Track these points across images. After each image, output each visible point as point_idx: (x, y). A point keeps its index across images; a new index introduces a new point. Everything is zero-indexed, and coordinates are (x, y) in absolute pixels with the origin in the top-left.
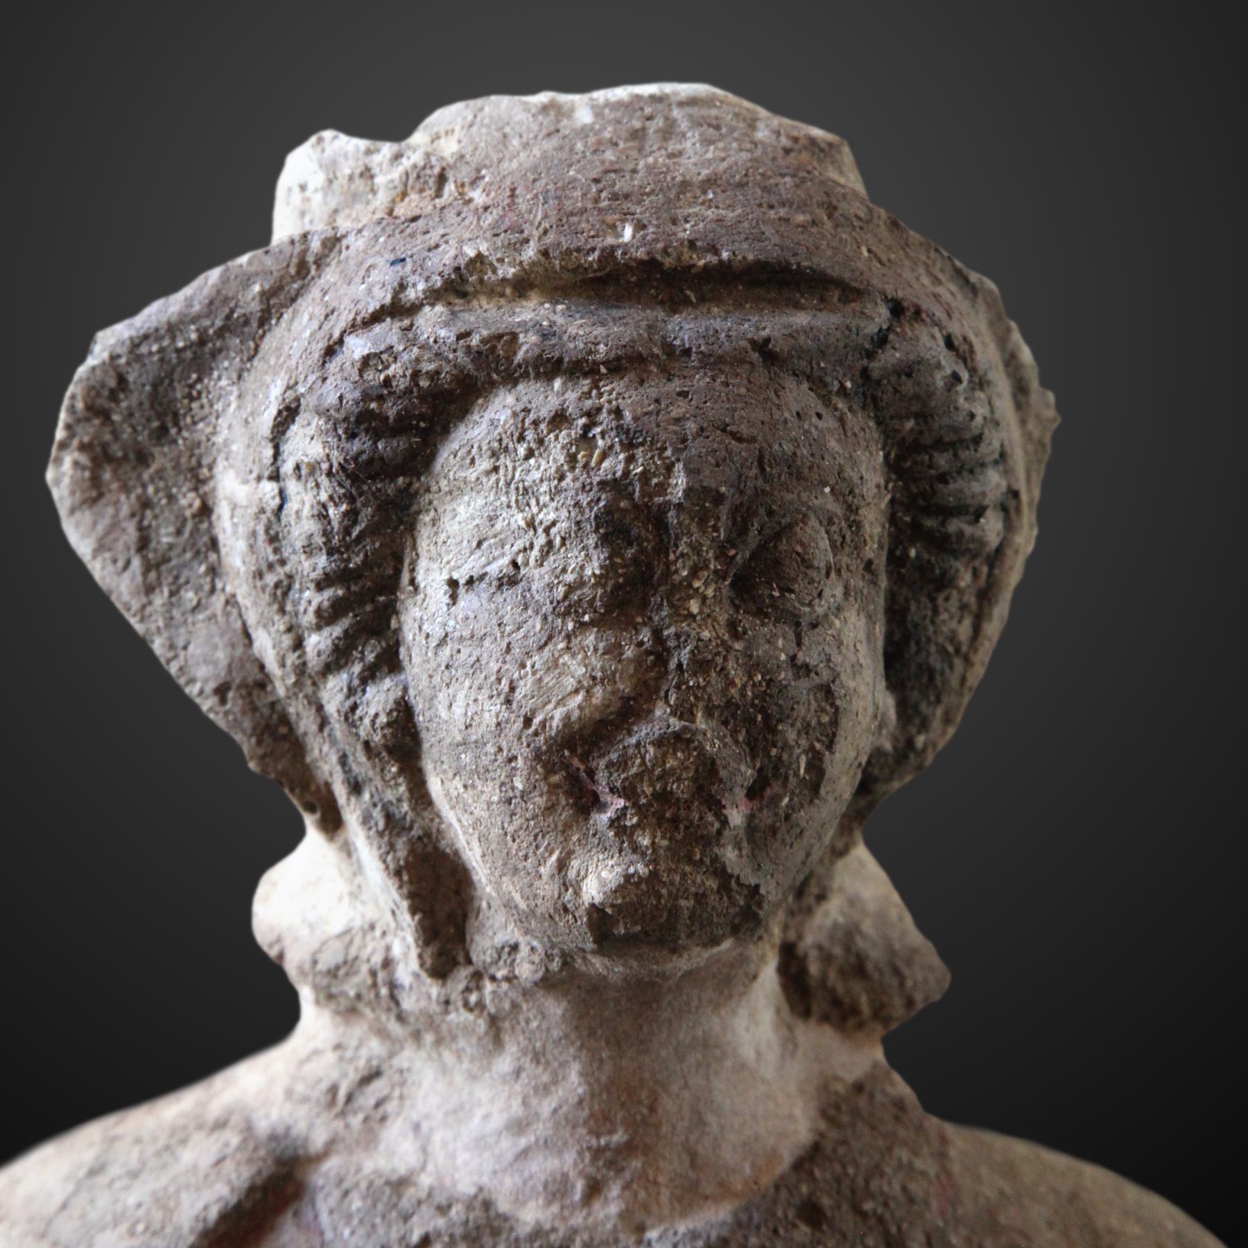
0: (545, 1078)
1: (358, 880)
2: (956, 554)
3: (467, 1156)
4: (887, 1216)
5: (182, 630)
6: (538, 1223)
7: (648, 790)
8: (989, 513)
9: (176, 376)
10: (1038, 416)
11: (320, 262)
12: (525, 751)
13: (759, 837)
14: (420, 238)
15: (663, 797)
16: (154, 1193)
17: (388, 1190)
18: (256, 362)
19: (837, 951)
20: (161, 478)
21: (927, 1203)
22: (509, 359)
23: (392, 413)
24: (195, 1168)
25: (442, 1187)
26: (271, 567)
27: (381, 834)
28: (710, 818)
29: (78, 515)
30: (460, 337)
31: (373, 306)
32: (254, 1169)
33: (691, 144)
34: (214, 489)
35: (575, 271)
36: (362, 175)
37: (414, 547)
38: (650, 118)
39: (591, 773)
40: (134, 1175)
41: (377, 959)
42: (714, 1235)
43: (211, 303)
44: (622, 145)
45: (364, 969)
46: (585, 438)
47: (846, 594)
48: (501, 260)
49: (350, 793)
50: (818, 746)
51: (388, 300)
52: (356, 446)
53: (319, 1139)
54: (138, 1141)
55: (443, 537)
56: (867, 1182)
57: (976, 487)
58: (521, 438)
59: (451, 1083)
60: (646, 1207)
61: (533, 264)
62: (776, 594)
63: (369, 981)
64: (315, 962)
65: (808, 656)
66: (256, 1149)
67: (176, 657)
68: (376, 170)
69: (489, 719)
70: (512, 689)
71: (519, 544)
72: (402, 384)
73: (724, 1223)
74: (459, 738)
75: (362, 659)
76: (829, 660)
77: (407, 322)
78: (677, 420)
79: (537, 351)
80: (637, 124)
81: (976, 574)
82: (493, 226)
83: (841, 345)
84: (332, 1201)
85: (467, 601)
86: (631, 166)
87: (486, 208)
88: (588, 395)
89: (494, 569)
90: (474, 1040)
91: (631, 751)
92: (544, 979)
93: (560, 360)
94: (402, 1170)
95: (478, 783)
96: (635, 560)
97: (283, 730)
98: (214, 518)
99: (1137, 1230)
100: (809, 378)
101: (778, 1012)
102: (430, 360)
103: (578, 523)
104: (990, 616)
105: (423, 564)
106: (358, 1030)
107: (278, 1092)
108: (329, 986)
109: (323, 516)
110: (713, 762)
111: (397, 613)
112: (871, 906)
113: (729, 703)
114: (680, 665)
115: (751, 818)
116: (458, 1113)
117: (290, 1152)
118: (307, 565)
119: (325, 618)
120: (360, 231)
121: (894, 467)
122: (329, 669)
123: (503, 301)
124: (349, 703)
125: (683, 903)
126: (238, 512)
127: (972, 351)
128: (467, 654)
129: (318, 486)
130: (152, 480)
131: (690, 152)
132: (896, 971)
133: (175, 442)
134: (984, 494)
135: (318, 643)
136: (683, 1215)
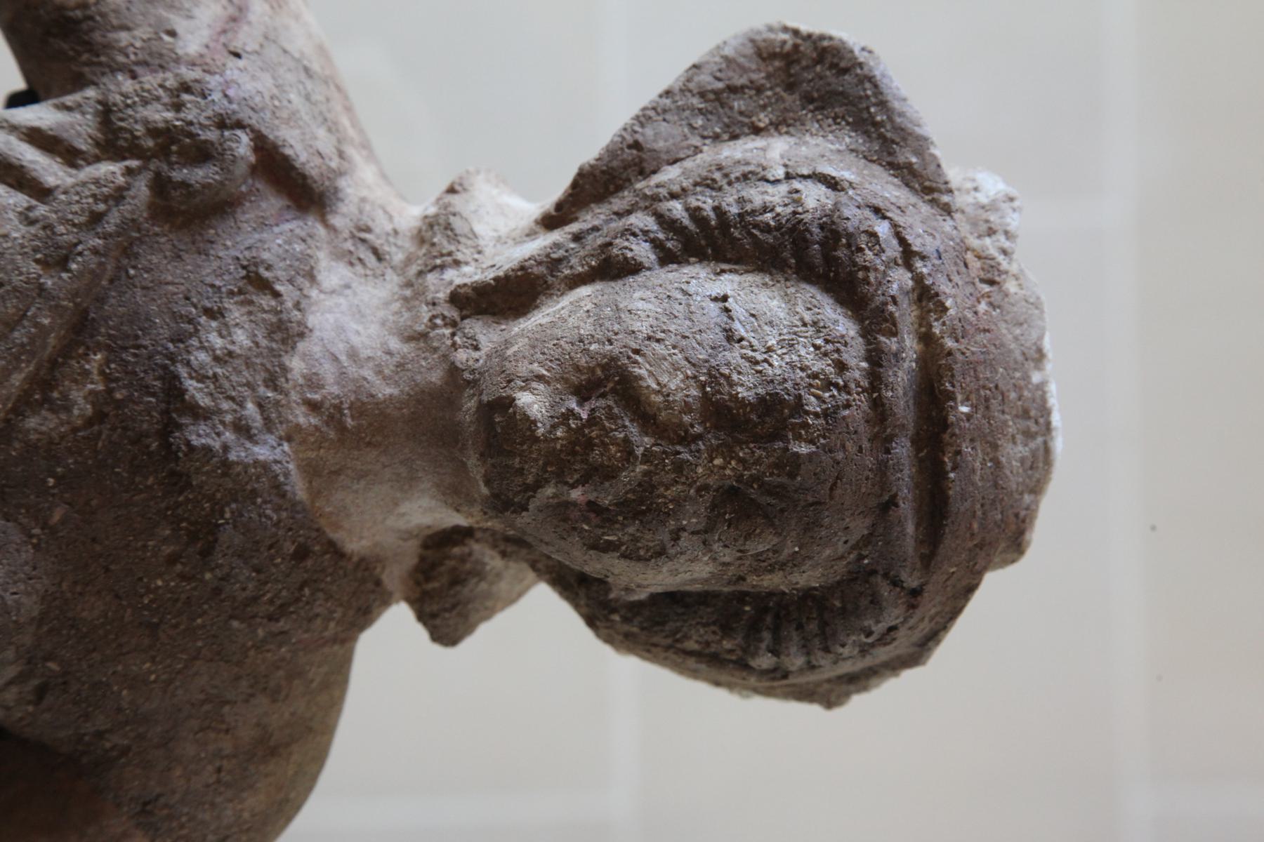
0: (387, 372)
1: (510, 242)
3: (332, 321)
4: (301, 604)
5: (676, 118)
6: (291, 370)
7: (593, 434)
8: (775, 659)
9: (850, 108)
10: (831, 691)
11: (934, 202)
12: (617, 351)
13: (562, 509)
14: (954, 269)
15: (589, 445)
16: (298, 111)
17: (307, 268)
18: (863, 161)
19: (468, 566)
20: (777, 100)
21: (306, 631)
22: (880, 331)
23: (839, 253)
24: (316, 138)
25: (311, 305)
27: (548, 255)
28: (576, 476)
29: (750, 45)
30: (893, 297)
31: (910, 239)
32: (316, 178)
34: (772, 136)
35: (938, 373)
36: (990, 228)
37: (747, 272)
38: (1037, 422)
39: (603, 396)
40: (308, 98)
41: (459, 256)
42: (288, 488)
43: (902, 130)
44: (1020, 403)
45: (453, 248)
46: (829, 385)
47: (724, 564)
48: (944, 324)
49: (573, 234)
50: (624, 548)
51: (915, 249)
52: (815, 230)
53: (336, 221)
54: (328, 100)
55: (756, 291)
56: (322, 590)
57: (793, 650)
58: (827, 341)
59: (378, 308)
60: (304, 442)
61: (942, 346)
62: (727, 517)
63: (444, 251)
64: (454, 215)
66: (329, 178)
67: (658, 114)
68: (994, 238)
69: (636, 326)
70: (658, 341)
71: (755, 342)
72: (859, 260)
73: (295, 494)
74: (621, 306)
75: (668, 239)
76: (681, 553)
77: (900, 262)
78: (843, 446)
79: (886, 350)
80: (1033, 413)
81: (730, 651)
82: (965, 317)
83: (894, 556)
84: (298, 231)
85: (714, 308)
86: (1007, 410)
87: (976, 313)
88: (858, 385)
89: (737, 326)
90: (409, 323)
91: (620, 422)
92: (456, 368)
93: (881, 366)
94: (319, 278)
95: (591, 320)
96: (748, 421)
97: (612, 188)
98: (753, 136)
99: (290, 773)
100: (871, 534)
101: (429, 527)
102: (876, 278)
103: (772, 381)
104: (701, 662)
105: (736, 278)
106: (410, 246)
107: (364, 193)
108: (439, 224)
109: (765, 209)
110: (614, 477)
111: (700, 261)
113: (654, 487)
114: (679, 453)
115: (575, 504)
117: (328, 202)
118: (731, 200)
119: (695, 213)
120: (956, 228)
121: (807, 595)
122: (660, 218)
123: (916, 326)
124: (637, 231)
125: (517, 460)
126: (761, 153)
127: (885, 644)
128: (679, 309)
129: (786, 205)
130: (775, 94)
131: (1016, 450)
132: (454, 606)
133: (804, 109)
134: (788, 655)
135: (676, 209)
136: (298, 467)
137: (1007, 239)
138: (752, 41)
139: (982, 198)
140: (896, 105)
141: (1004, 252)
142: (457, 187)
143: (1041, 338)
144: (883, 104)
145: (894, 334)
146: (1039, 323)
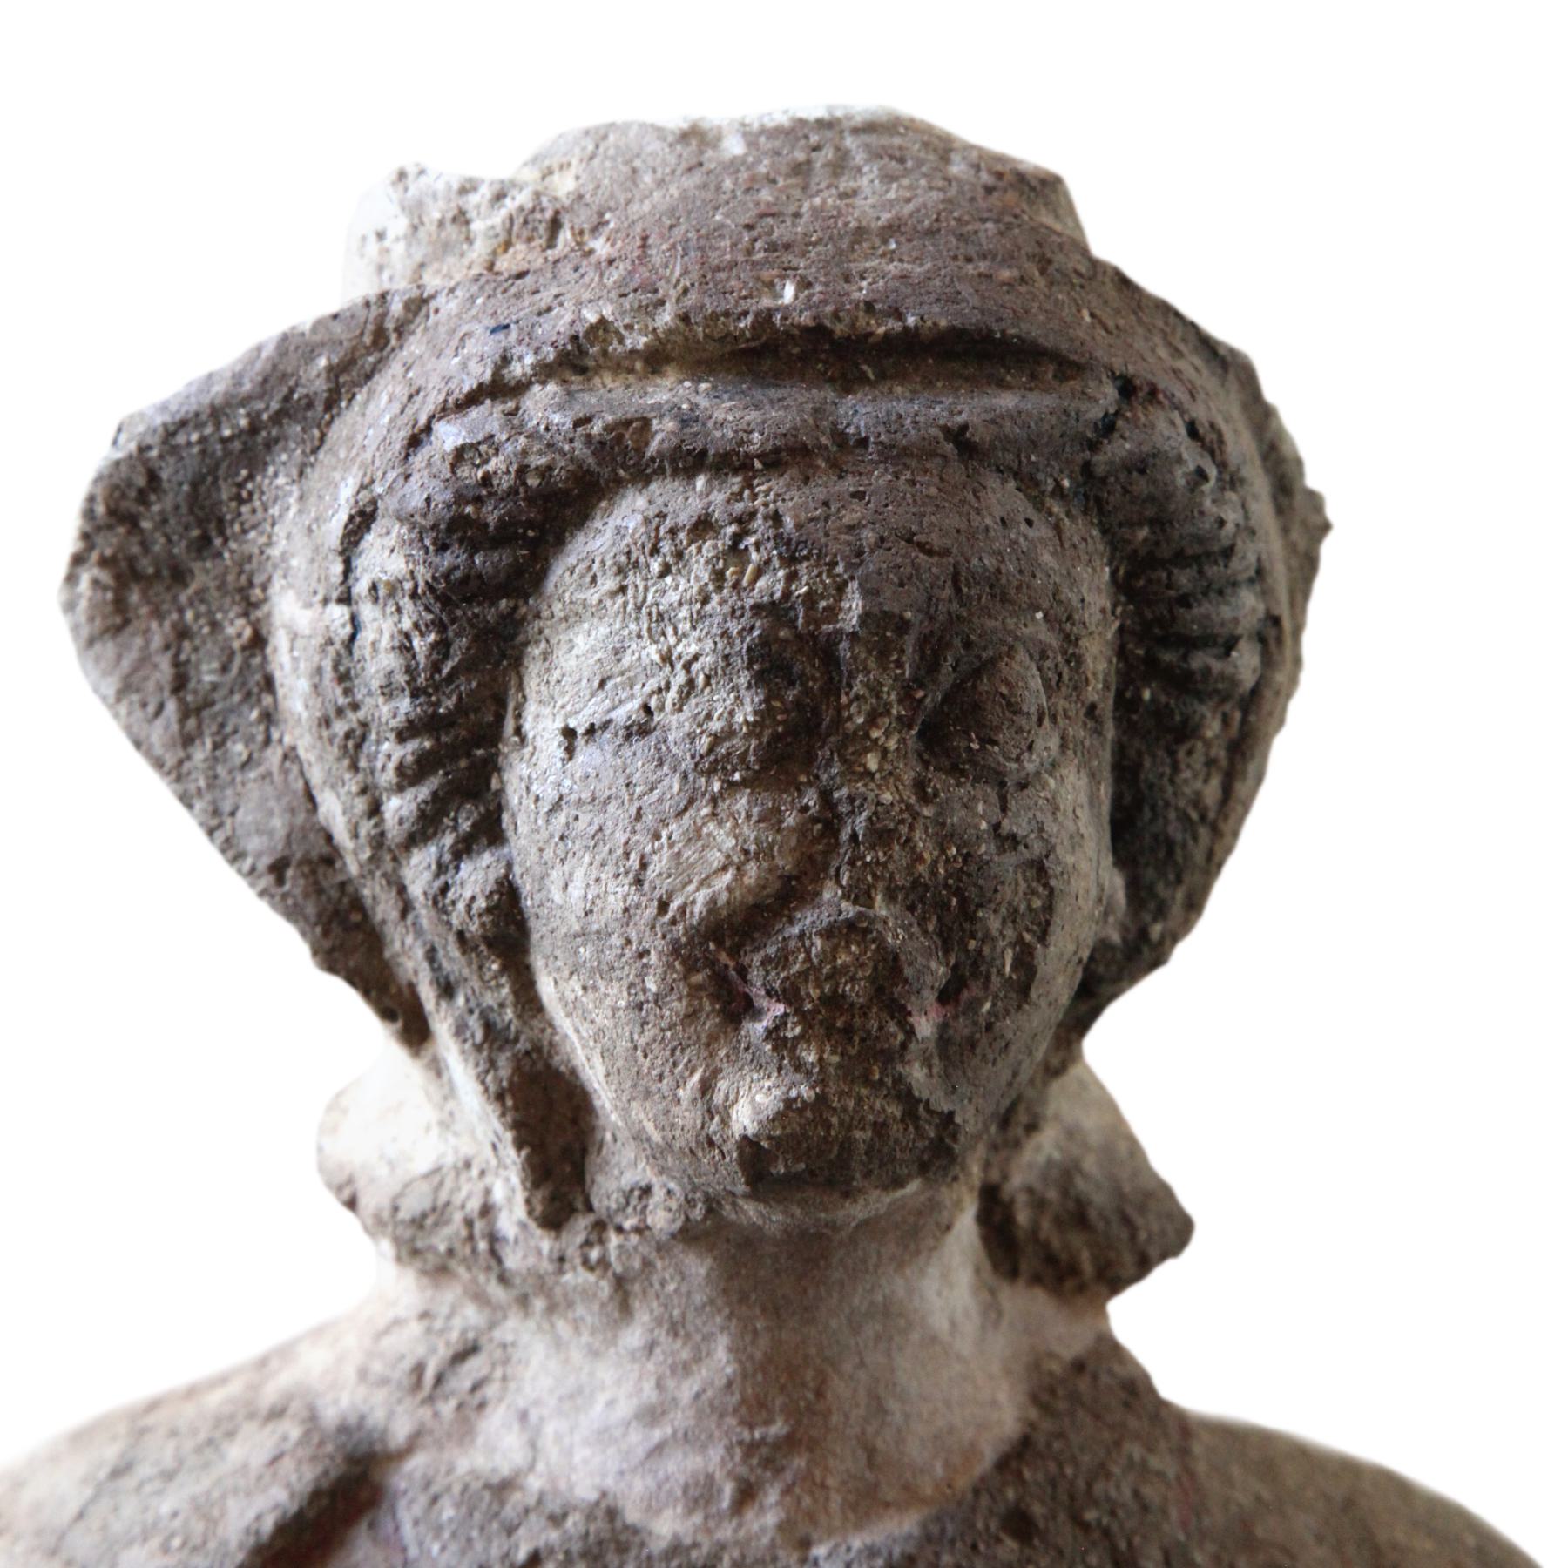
0: (685, 1355)
1: (450, 1105)
2: (1201, 697)
3: (587, 1452)
4: (1115, 1527)
5: (229, 792)
6: (676, 1536)
7: (815, 993)
8: (1243, 645)
9: (221, 472)
10: (1304, 523)
11: (402, 330)
12: (660, 943)
13: (953, 1052)
14: (527, 300)
15: (834, 1001)
16: (194, 1499)
17: (487, 1495)
18: (321, 455)
19: (1052, 1194)
20: (202, 601)
21: (1164, 1512)
22: (640, 451)
23: (492, 519)
24: (245, 1467)
25: (556, 1492)
26: (340, 712)
27: (478, 1048)
28: (892, 1027)
29: (98, 647)
30: (578, 423)
31: (469, 384)
32: (319, 1469)
33: (868, 181)
34: (269, 615)
35: (722, 340)
36: (454, 220)
37: (520, 687)
38: (816, 149)
39: (743, 972)
40: (168, 1476)
41: (474, 1205)
42: (897, 1552)
43: (265, 381)
44: (781, 182)
45: (458, 1217)
46: (735, 551)
47: (1063, 746)
48: (629, 327)
49: (439, 997)
50: (1028, 937)
51: (487, 377)
52: (447, 560)
53: (400, 1432)
54: (174, 1433)
55: (556, 674)
56: (1089, 1485)
57: (1226, 612)
58: (655, 551)
59: (567, 1361)
60: (811, 1517)
61: (670, 332)
62: (975, 746)
63: (464, 1233)
64: (396, 1209)
65: (1015, 824)
66: (321, 1443)
67: (221, 825)
68: (472, 214)
69: (615, 903)
70: (644, 866)
71: (653, 684)
72: (504, 483)
73: (909, 1537)
74: (577, 927)
75: (455, 828)
76: (1041, 830)
77: (511, 405)
78: (851, 528)
79: (675, 441)
80: (800, 156)
81: (1226, 721)
82: (620, 284)
83: (1057, 433)
84: (417, 1510)
85: (587, 755)
86: (792, 209)
87: (611, 262)
88: (738, 496)
89: (620, 715)
90: (596, 1307)
91: (792, 944)
92: (684, 1231)
93: (704, 453)
94: (505, 1471)
95: (601, 984)
96: (798, 704)
97: (356, 917)
98: (269, 650)
99: (1429, 1545)
100: (1016, 475)
101: (977, 1271)
102: (540, 453)
103: (726, 657)
105: (531, 708)
106: (450, 1294)
107: (350, 1372)
108: (413, 1239)
109: (405, 648)
110: (896, 958)
111: (499, 770)
112: (1095, 1139)
113: (916, 883)
114: (854, 836)
115: (943, 1027)
116: (575, 1398)
117: (364, 1448)
118: (385, 710)
119: (408, 777)
120: (452, 290)
121: (1123, 587)
122: (413, 840)
123: (631, 378)
124: (438, 884)
125: (858, 1134)
126: (300, 643)
127: (1221, 441)
128: (587, 822)
129: (399, 610)
130: (191, 604)
131: (867, 191)
132: (1126, 1220)
133: (219, 555)
134: (1236, 621)
135: (399, 808)
136: (859, 1527)
137: (475, 189)
138: (91, 642)
139: (398, 226)
140: (219, 389)
141: (499, 197)
142: (346, 1194)
143: (660, 132)
144: (217, 413)
145: (757, 1515)
146: (632, 133)
